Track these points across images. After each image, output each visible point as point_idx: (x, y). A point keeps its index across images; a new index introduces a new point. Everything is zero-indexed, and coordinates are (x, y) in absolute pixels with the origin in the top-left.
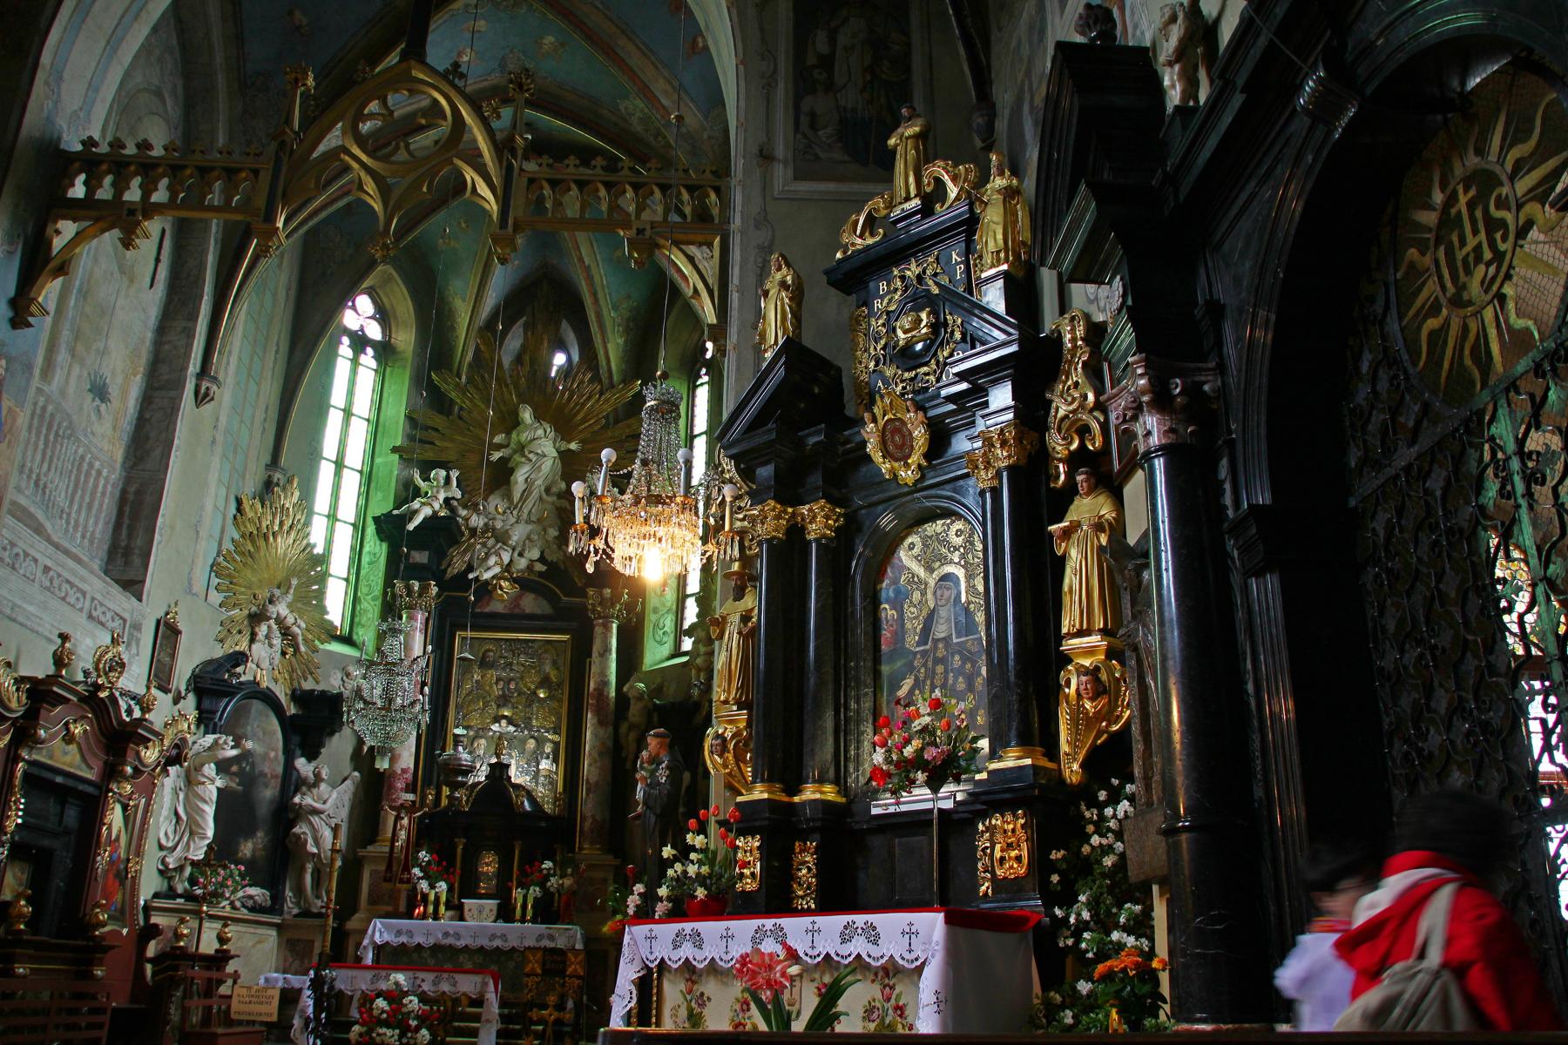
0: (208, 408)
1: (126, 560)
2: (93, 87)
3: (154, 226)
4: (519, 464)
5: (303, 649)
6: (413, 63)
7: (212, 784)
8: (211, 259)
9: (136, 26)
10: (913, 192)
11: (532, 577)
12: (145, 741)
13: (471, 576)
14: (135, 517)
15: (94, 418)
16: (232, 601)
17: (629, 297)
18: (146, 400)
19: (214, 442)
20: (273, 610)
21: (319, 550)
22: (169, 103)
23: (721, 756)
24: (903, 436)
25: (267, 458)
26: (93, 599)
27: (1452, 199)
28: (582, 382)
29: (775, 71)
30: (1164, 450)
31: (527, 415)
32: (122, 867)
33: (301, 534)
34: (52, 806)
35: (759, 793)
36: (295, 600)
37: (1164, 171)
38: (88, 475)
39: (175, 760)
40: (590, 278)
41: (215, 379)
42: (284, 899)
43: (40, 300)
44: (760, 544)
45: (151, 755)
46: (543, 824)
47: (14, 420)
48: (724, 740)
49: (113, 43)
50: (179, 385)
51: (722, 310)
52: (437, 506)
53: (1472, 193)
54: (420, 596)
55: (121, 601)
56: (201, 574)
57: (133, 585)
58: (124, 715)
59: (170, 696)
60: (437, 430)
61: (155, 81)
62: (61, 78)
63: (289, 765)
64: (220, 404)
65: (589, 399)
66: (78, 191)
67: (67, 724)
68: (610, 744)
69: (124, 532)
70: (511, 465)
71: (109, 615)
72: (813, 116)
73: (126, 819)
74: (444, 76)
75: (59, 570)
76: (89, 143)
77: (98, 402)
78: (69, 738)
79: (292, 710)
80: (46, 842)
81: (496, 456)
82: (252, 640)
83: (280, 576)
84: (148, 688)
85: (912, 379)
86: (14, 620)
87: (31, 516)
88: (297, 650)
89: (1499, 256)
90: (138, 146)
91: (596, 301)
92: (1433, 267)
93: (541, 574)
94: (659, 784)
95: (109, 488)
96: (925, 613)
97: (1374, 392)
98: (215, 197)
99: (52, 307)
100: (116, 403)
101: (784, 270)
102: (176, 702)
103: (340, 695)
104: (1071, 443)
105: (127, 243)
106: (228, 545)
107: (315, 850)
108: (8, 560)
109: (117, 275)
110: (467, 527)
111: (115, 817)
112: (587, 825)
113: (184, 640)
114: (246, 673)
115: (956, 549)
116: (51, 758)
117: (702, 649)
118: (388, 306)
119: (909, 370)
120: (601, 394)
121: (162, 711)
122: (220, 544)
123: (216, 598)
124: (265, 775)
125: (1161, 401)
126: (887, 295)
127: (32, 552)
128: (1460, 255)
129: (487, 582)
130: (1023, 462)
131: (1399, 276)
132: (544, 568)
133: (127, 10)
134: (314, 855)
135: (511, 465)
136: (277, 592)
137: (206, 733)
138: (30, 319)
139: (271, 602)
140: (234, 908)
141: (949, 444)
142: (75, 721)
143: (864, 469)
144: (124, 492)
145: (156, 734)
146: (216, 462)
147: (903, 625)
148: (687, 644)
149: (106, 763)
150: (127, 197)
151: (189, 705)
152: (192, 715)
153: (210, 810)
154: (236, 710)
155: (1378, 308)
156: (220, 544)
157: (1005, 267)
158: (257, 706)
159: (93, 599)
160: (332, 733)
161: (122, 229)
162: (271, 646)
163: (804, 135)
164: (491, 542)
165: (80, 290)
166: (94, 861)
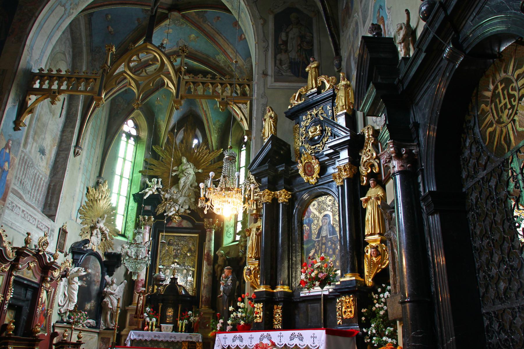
0: (78, 157)
1: (50, 209)
2: (43, 52)
3: (61, 97)
5: (108, 238)
6: (148, 43)
7: (77, 284)
10: (314, 86)
13: (165, 214)
14: (53, 194)
15: (40, 161)
16: (85, 222)
17: (219, 121)
18: (58, 155)
19: (80, 169)
21: (114, 205)
22: (67, 56)
23: (249, 276)
25: (97, 174)
26: (38, 221)
27: (496, 88)
28: (203, 149)
29: (268, 46)
30: (399, 172)
31: (184, 160)
32: (46, 312)
34: (23, 291)
37: (399, 79)
38: (38, 179)
41: (80, 148)
44: (263, 204)
45: (56, 274)
47: (14, 161)
48: (250, 270)
49: (50, 38)
50: (69, 150)
51: (250, 125)
52: (154, 191)
53: (503, 85)
55: (47, 222)
56: (75, 213)
57: (52, 216)
58: (48, 260)
59: (63, 254)
61: (63, 50)
62: (32, 49)
63: (103, 278)
64: (82, 156)
65: (205, 155)
66: (37, 85)
67: (28, 263)
68: (212, 271)
69: (49, 199)
71: (44, 226)
72: (281, 60)
73: (48, 296)
74: (158, 48)
75: (27, 211)
76: (41, 70)
77: (41, 155)
78: (29, 268)
79: (104, 259)
80: (20, 303)
81: (174, 174)
82: (91, 235)
83: (101, 214)
85: (314, 149)
86: (12, 228)
87: (18, 193)
89: (513, 107)
90: (57, 71)
91: (208, 122)
92: (490, 110)
93: (189, 214)
94: (228, 285)
95: (45, 184)
96: (318, 228)
97: (471, 152)
99: (27, 124)
100: (47, 156)
101: (271, 112)
103: (121, 254)
104: (368, 170)
105: (53, 103)
107: (111, 307)
108: (10, 208)
112: (204, 299)
113: (68, 235)
114: (89, 246)
115: (329, 206)
116: (23, 275)
117: (243, 239)
119: (313, 146)
120: (209, 153)
121: (61, 259)
122: (81, 203)
123: (79, 221)
124: (95, 281)
125: (398, 156)
126: (306, 120)
127: (19, 205)
128: (499, 106)
130: (352, 176)
131: (479, 113)
132: (190, 212)
133: (55, 27)
136: (100, 219)
137: (75, 267)
139: (98, 222)
140: (83, 326)
141: (29, 96)
143: (298, 179)
144: (49, 185)
145: (58, 267)
146: (80, 175)
147: (311, 231)
149: (41, 276)
150: (53, 87)
152: (71, 260)
153: (76, 293)
154: (85, 259)
155: (472, 124)
156: (81, 203)
157: (345, 111)
158: (92, 257)
159: (38, 221)
160: (118, 267)
161: (51, 98)
162: (98, 237)
163: (278, 68)
164: (172, 203)
165: (37, 118)
166: (36, 310)
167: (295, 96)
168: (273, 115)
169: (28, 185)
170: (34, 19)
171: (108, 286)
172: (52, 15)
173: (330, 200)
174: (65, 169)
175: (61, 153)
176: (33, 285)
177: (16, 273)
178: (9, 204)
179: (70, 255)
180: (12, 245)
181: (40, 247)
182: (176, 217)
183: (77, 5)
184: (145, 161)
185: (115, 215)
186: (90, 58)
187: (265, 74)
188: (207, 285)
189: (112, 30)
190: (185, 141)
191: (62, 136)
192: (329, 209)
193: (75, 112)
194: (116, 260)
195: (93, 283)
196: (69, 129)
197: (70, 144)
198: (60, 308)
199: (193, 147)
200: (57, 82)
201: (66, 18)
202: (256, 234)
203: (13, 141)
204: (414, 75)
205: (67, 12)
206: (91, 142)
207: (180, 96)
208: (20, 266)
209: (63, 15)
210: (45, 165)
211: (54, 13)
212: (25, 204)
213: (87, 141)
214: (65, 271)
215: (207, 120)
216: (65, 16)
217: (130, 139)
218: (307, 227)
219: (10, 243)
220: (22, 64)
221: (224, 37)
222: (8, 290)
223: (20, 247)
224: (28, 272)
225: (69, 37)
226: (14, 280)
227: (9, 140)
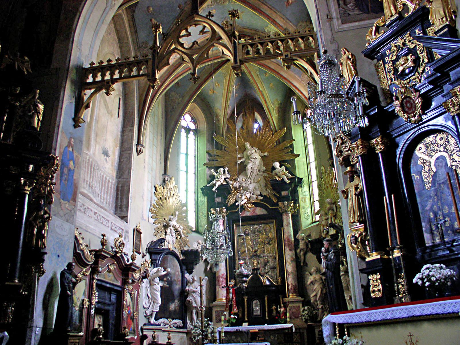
0: (141, 155)
1: (121, 207)
2: (91, 47)
3: (115, 86)
5: (183, 236)
6: (195, 15)
7: (158, 285)
8: (136, 106)
9: (103, 25)
10: (393, 12)
11: (258, 202)
12: (134, 270)
13: (237, 204)
14: (122, 195)
16: (157, 222)
17: (277, 100)
18: (121, 155)
21: (184, 202)
23: (355, 244)
24: (411, 104)
25: (163, 172)
26: (112, 223)
28: (265, 132)
31: (248, 145)
32: (132, 315)
34: (106, 294)
35: (375, 256)
38: (105, 182)
39: (145, 277)
40: (263, 95)
41: (142, 146)
42: (187, 323)
43: (82, 117)
44: (357, 157)
45: (137, 275)
46: (274, 289)
47: (78, 160)
48: (356, 237)
49: (96, 32)
50: (131, 148)
52: (222, 182)
54: (220, 213)
55: (120, 223)
56: (146, 213)
57: (124, 218)
58: (126, 262)
59: (141, 255)
61: (112, 50)
62: (81, 44)
63: (183, 277)
64: (145, 154)
65: (268, 137)
66: (90, 80)
67: (108, 266)
68: (294, 257)
69: (119, 200)
70: (245, 164)
71: (118, 228)
73: (131, 298)
74: (206, 17)
75: (100, 213)
77: (106, 157)
78: (110, 271)
79: (182, 257)
80: (107, 308)
81: (239, 162)
82: (166, 234)
83: (172, 212)
84: (133, 252)
85: (408, 83)
86: (87, 231)
87: (89, 196)
88: (181, 236)
90: (108, 61)
91: (266, 102)
93: (261, 200)
94: (331, 259)
95: (113, 186)
96: (432, 174)
100: (111, 157)
102: (143, 257)
103: (197, 250)
105: (107, 94)
106: (154, 203)
107: (196, 305)
108: (82, 210)
109: (107, 114)
110: (233, 187)
111: (128, 297)
112: (290, 287)
113: (143, 235)
114: (165, 245)
115: (441, 146)
116: (105, 278)
117: (324, 218)
118: (195, 117)
120: (273, 134)
121: (139, 261)
122: (151, 202)
123: (152, 221)
124: (176, 281)
127: (90, 207)
129: (243, 206)
132: (262, 198)
133: (99, 21)
134: (195, 307)
135: (245, 164)
136: (172, 217)
137: (154, 267)
138: (80, 124)
139: (170, 221)
140: (171, 327)
141: (84, 90)
142: (111, 265)
143: (395, 122)
144: (118, 187)
145: (138, 268)
146: (146, 174)
147: (423, 180)
148: (318, 218)
149: (123, 279)
150: (106, 78)
151: (148, 257)
152: (149, 261)
153: (159, 294)
154: (163, 259)
158: (170, 257)
159: (112, 223)
160: (196, 264)
161: (105, 89)
162: (172, 236)
163: (343, 8)
164: (242, 192)
165: (96, 119)
166: (123, 314)
167: (372, 31)
168: (350, 57)
169: (97, 187)
170: (78, 14)
171: (189, 284)
172: (95, 9)
173: (441, 139)
174: (130, 169)
175: (124, 153)
176: (116, 288)
177: (97, 276)
178: (81, 207)
179: (148, 256)
180: (89, 248)
181: (116, 248)
182: (249, 205)
184: (208, 153)
185: (186, 212)
187: (329, 18)
188: (292, 272)
191: (122, 136)
192: (442, 150)
193: (131, 111)
194: (193, 257)
195: (174, 282)
196: (129, 129)
197: (132, 143)
198: (145, 310)
199: (255, 132)
200: (109, 72)
201: (109, 10)
202: (355, 194)
204: (449, 60)
205: (109, 4)
206: (152, 140)
207: (238, 61)
208: (100, 269)
210: (111, 167)
211: (97, 6)
212: (96, 206)
213: (148, 139)
214: (145, 272)
215: (265, 101)
216: (107, 9)
217: (189, 133)
218: (416, 177)
219: (87, 246)
220: (74, 60)
221: (270, 5)
222: (92, 294)
223: (97, 249)
224: (108, 274)
225: (116, 37)
226: (97, 284)
227: (71, 138)
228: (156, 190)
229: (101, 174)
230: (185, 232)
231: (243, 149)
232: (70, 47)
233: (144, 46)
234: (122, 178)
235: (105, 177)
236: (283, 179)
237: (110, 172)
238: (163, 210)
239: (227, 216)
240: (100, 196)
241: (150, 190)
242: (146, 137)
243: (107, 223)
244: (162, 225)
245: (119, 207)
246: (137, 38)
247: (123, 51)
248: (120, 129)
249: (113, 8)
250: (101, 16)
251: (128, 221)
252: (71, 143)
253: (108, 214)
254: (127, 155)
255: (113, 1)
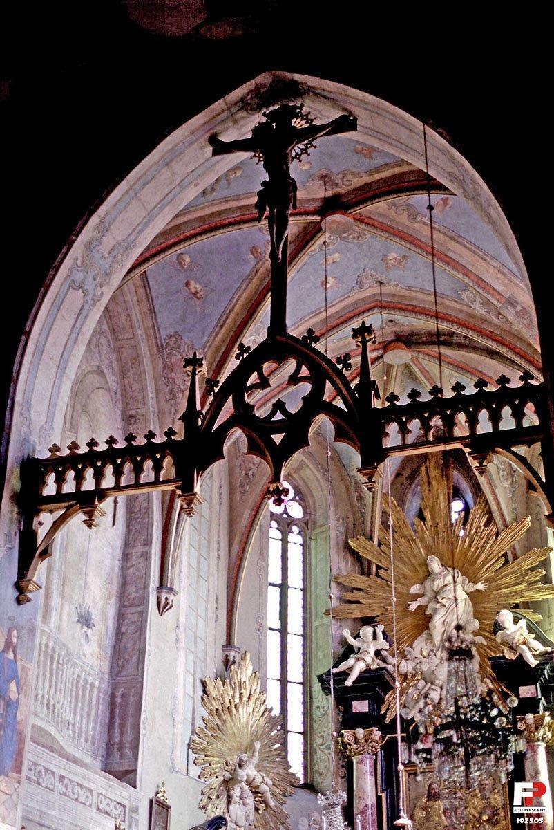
0: (169, 614)
3: (106, 505)
4: (436, 610)
5: (272, 803)
9: (76, 347)
15: (83, 642)
18: (121, 617)
19: (177, 640)
20: (242, 773)
31: (435, 565)
33: (259, 702)
36: (261, 761)
38: (84, 688)
43: (35, 579)
47: (27, 675)
49: (62, 367)
50: (144, 601)
52: (369, 660)
55: (120, 791)
56: (181, 752)
57: (127, 776)
60: (360, 590)
61: (96, 363)
62: (30, 406)
66: (50, 489)
69: (117, 730)
71: (112, 804)
75: (71, 776)
76: (55, 449)
77: (85, 627)
81: (413, 606)
82: (229, 803)
83: (246, 741)
88: (267, 805)
95: (102, 696)
98: (148, 475)
99: (43, 581)
105: (90, 524)
106: (199, 724)
113: (173, 814)
120: (498, 534)
122: (193, 724)
123: (195, 771)
127: (50, 767)
138: (29, 595)
139: (240, 766)
144: (113, 696)
146: (182, 654)
156: (193, 724)
159: (99, 794)
162: (245, 805)
165: (62, 543)
170: (23, 338)
172: (59, 316)
174: (142, 652)
175: (129, 610)
178: (30, 769)
183: (108, 274)
186: (161, 366)
189: (199, 287)
190: (427, 514)
191: (124, 569)
196: (138, 550)
197: (146, 587)
203: (19, 629)
205: (89, 298)
209: (83, 306)
210: (96, 651)
211: (63, 310)
216: (86, 308)
221: (470, 243)
227: (11, 629)
228: (205, 692)
229: (73, 673)
230: (277, 791)
231: (422, 574)
232: (7, 422)
233: (171, 344)
234: (123, 674)
235: (82, 677)
236: (521, 655)
237: (96, 662)
238: (223, 741)
239: (382, 748)
240: (71, 727)
241: (191, 693)
242: (181, 561)
243: (87, 797)
244: (221, 778)
245: (116, 746)
246: (155, 327)
247: (123, 359)
248: (118, 553)
249: (98, 304)
250: (72, 329)
251: (138, 784)
252: (12, 643)
253: (90, 774)
254: (135, 617)
255: (99, 289)
